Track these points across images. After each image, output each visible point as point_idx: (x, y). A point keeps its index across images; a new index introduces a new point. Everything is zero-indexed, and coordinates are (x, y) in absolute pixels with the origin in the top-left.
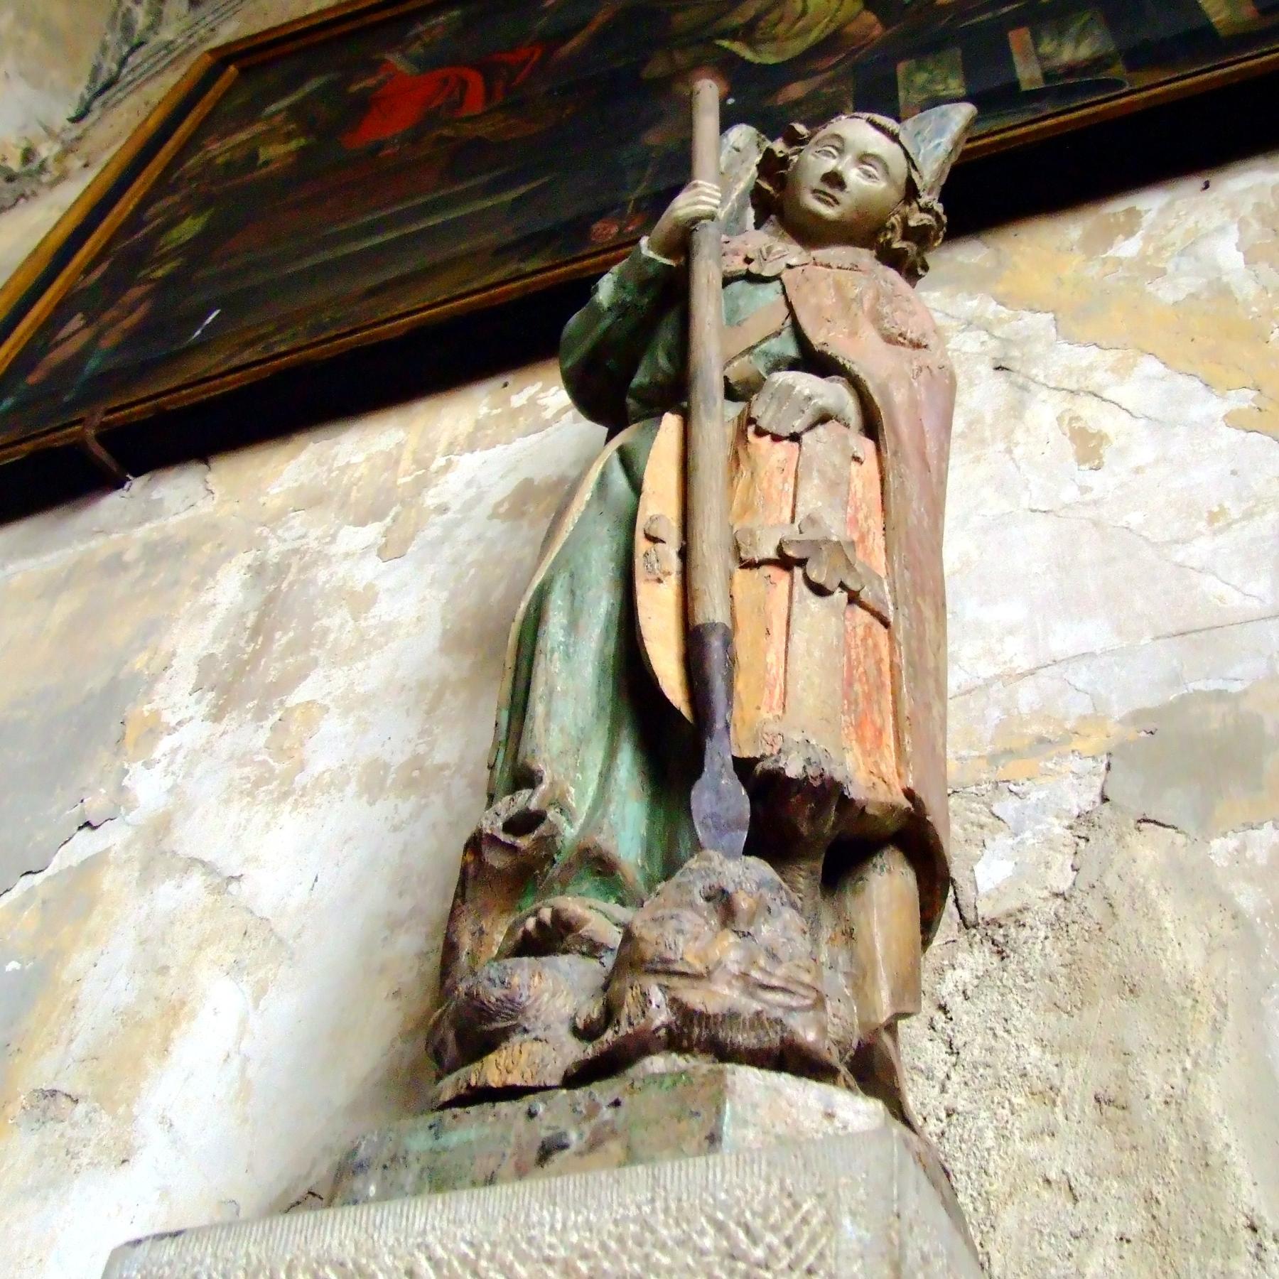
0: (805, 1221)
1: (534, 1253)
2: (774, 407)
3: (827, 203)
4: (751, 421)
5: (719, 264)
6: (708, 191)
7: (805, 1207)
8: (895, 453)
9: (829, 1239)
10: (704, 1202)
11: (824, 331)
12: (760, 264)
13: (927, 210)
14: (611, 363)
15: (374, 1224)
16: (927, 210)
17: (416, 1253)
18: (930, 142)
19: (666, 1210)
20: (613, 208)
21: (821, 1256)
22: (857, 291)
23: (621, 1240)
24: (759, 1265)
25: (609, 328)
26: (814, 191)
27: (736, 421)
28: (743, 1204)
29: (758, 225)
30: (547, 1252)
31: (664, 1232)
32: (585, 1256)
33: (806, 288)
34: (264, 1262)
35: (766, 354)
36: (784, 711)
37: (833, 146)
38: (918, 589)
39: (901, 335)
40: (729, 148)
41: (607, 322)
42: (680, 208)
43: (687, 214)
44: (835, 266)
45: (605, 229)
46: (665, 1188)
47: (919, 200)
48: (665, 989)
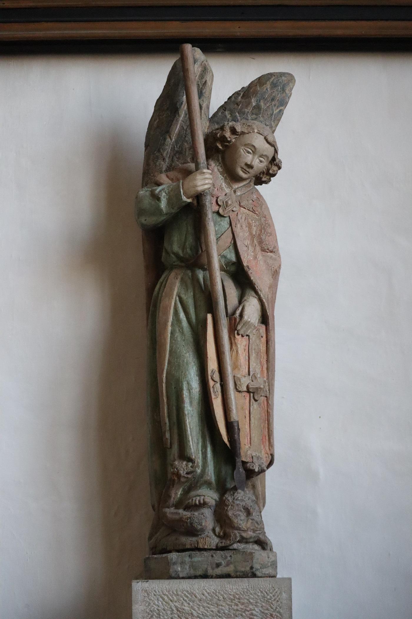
0: (276, 592)
1: (227, 593)
3: (246, 173)
7: (276, 590)
9: (281, 596)
10: (258, 587)
15: (193, 584)
17: (203, 591)
19: (251, 588)
21: (279, 599)
23: (244, 592)
24: (269, 599)
26: (242, 168)
28: (265, 588)
30: (230, 593)
31: (251, 591)
32: (238, 595)
34: (170, 589)
36: (251, 445)
46: (251, 583)
48: (239, 533)
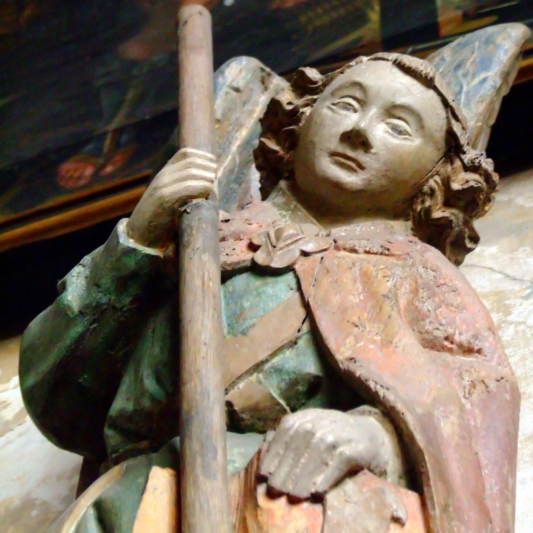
2: (289, 461)
3: (349, 169)
4: (262, 479)
5: (216, 254)
6: (199, 161)
8: (445, 508)
11: (350, 340)
12: (269, 254)
13: (473, 168)
14: (84, 379)
16: (473, 168)
18: (474, 76)
20: (87, 142)
22: (389, 284)
25: (82, 337)
26: (333, 154)
27: (242, 474)
29: (265, 194)
33: (325, 282)
35: (278, 370)
37: (355, 98)
38: (508, 501)
39: (447, 338)
40: (225, 89)
41: (77, 330)
42: (165, 186)
43: (174, 193)
44: (361, 250)
45: (76, 171)
47: (463, 157)
